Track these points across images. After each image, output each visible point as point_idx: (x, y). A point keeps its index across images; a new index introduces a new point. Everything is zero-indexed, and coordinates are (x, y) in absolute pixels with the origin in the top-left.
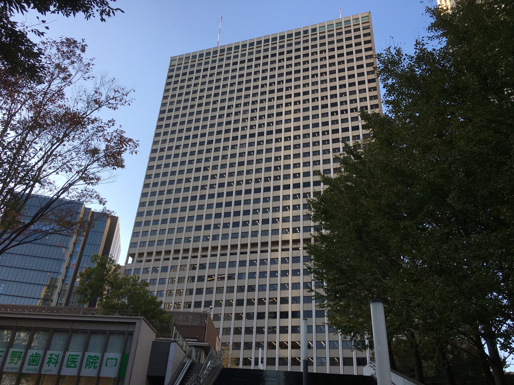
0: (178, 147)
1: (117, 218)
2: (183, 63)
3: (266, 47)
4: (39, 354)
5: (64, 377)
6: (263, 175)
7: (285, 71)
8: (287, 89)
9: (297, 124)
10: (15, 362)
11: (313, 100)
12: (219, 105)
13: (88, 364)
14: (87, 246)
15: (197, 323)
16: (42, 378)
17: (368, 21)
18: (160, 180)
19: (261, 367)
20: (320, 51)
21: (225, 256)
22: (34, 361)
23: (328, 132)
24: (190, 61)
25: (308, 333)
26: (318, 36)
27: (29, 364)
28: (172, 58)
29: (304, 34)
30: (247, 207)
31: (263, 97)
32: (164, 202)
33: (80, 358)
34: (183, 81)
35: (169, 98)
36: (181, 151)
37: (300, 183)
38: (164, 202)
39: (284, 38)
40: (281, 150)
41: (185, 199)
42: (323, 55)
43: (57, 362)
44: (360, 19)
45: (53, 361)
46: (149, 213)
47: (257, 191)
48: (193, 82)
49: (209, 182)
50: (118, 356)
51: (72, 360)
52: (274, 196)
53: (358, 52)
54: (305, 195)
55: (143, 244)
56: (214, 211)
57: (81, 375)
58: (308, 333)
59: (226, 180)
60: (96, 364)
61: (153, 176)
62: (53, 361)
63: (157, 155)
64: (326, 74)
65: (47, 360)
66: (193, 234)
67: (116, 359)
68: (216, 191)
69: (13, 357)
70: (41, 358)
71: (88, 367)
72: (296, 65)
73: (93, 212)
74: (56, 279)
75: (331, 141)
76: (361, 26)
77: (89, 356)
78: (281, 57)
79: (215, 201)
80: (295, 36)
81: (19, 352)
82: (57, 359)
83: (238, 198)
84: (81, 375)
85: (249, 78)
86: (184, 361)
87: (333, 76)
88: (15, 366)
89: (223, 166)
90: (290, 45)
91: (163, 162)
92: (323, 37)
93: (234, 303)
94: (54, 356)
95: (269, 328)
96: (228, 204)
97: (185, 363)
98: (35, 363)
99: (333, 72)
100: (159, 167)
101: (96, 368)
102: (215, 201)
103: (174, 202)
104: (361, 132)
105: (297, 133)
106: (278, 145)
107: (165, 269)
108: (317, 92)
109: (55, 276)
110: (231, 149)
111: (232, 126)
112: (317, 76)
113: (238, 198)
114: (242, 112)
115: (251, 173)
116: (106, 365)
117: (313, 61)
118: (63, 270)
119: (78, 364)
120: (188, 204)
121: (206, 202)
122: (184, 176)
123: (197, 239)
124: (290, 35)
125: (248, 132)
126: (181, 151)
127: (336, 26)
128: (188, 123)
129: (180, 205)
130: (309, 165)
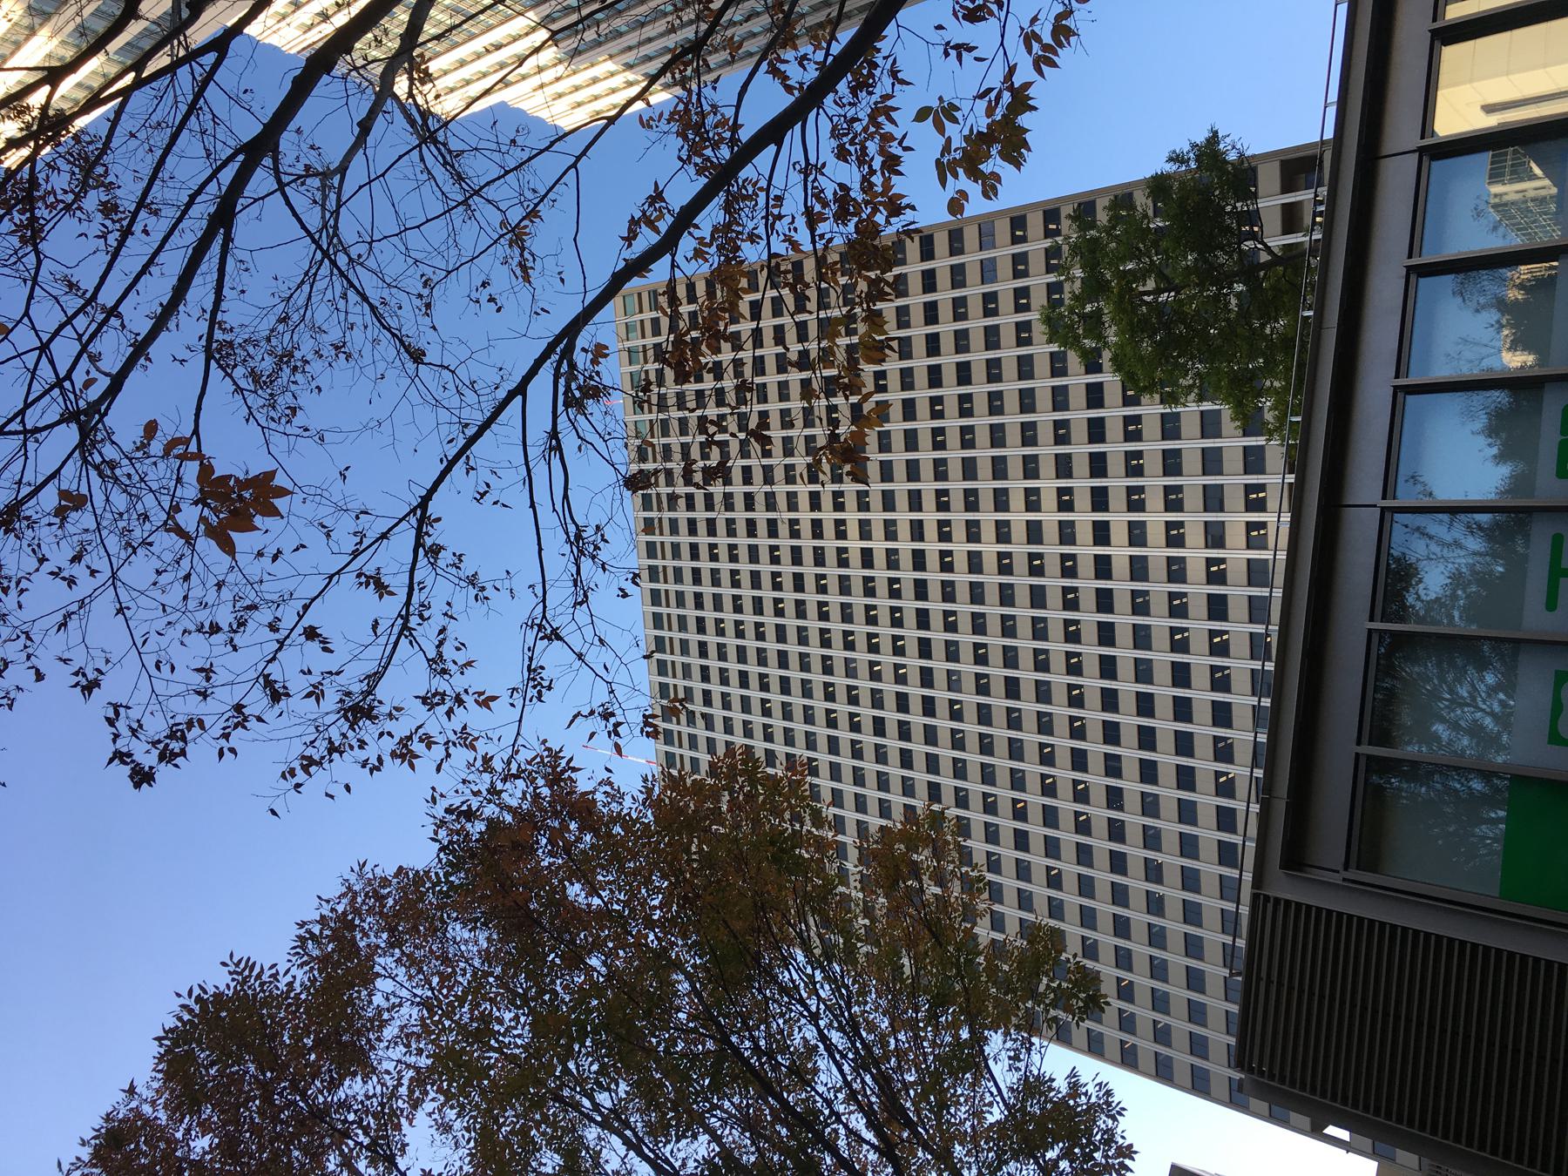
6: (1059, 679)
17: (636, 296)
20: (711, 560)
23: (943, 554)
30: (1163, 674)
37: (1092, 488)
40: (989, 706)
41: (1119, 895)
46: (1162, 1035)
47: (1106, 634)
49: (1066, 805)
52: (1132, 646)
54: (1132, 436)
56: (1168, 792)
59: (1063, 743)
64: (779, 574)
68: (1097, 780)
75: (969, 485)
76: (648, 315)
79: (1131, 785)
80: (662, 629)
83: (1129, 736)
87: (831, 557)
89: (1016, 750)
96: (1147, 738)
99: (759, 366)
102: (1131, 785)
103: (1126, 906)
110: (962, 721)
111: (891, 716)
112: (781, 601)
113: (1127, 703)
120: (1137, 884)
121: (1133, 819)
125: (913, 662)
129: (1138, 917)
130: (1044, 620)
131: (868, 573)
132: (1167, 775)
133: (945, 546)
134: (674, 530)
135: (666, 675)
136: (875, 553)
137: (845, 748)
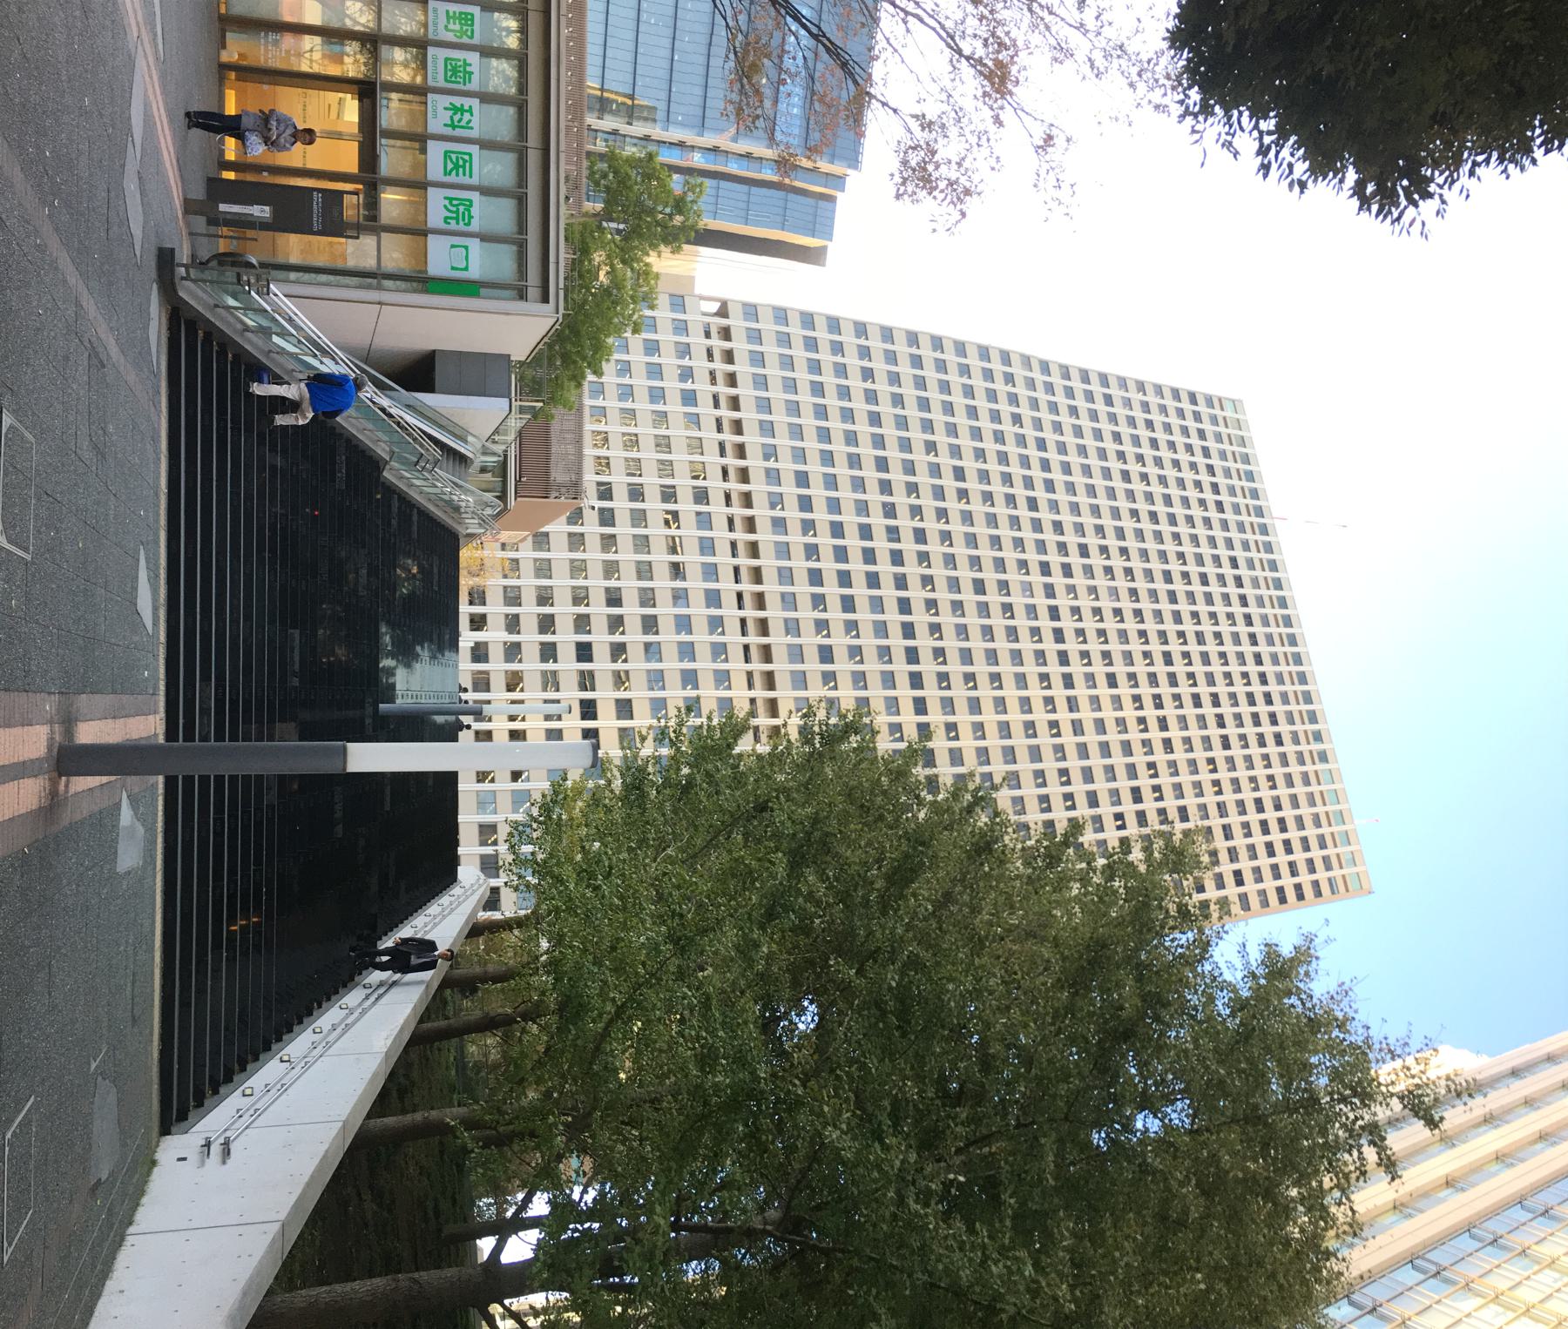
0: (1017, 419)
1: (824, 265)
2: (1230, 431)
3: (1277, 640)
4: (470, 81)
5: (424, 151)
7: (1222, 689)
8: (1177, 697)
9: (1089, 727)
10: (451, 26)
11: (1152, 766)
12: (1128, 524)
13: (454, 202)
14: (745, 188)
15: (558, 475)
16: (418, 98)
18: (930, 373)
19: (467, 638)
21: (736, 606)
22: (455, 71)
24: (1235, 448)
25: (549, 771)
26: (1309, 768)
27: (446, 60)
28: (1241, 401)
29: (1313, 733)
31: (1153, 637)
32: (868, 385)
33: (466, 180)
34: (1185, 431)
35: (1140, 396)
36: (1007, 427)
38: (868, 385)
39: (1300, 684)
40: (1018, 688)
42: (1263, 783)
43: (454, 128)
44: (1355, 870)
45: (456, 118)
48: (1183, 457)
50: (474, 273)
51: (461, 162)
53: (1275, 870)
55: (756, 336)
57: (430, 190)
58: (549, 771)
60: (453, 222)
61: (938, 355)
62: (456, 118)
63: (997, 366)
65: (457, 101)
66: (787, 466)
67: (466, 269)
69: (460, 19)
70: (461, 87)
71: (447, 202)
72: (1238, 717)
73: (831, 199)
74: (654, 121)
77: (471, 201)
78: (1255, 679)
80: (1308, 712)
81: (472, 31)
82: (462, 127)
84: (430, 190)
85: (1200, 598)
86: (470, 439)
88: (441, 27)
90: (1285, 698)
91: (978, 382)
92: (1306, 782)
93: (613, 583)
94: (467, 116)
95: (554, 673)
97: (466, 442)
98: (449, 74)
100: (965, 370)
101: (446, 222)
104: (1034, 817)
105: (1066, 728)
106: (1033, 681)
107: (689, 398)
108: (1197, 795)
109: (660, 115)
114: (1112, 584)
115: (954, 611)
116: (453, 246)
117: (1248, 759)
118: (675, 134)
119: (452, 179)
122: (941, 438)
123: (773, 476)
124: (1308, 698)
126: (1007, 427)
127: (1334, 812)
128: (1078, 446)
131: (1125, 737)
132: (984, 542)
133: (1043, 791)
134: (1300, 755)
135: (1298, 673)
136: (1125, 776)
137: (1235, 600)
